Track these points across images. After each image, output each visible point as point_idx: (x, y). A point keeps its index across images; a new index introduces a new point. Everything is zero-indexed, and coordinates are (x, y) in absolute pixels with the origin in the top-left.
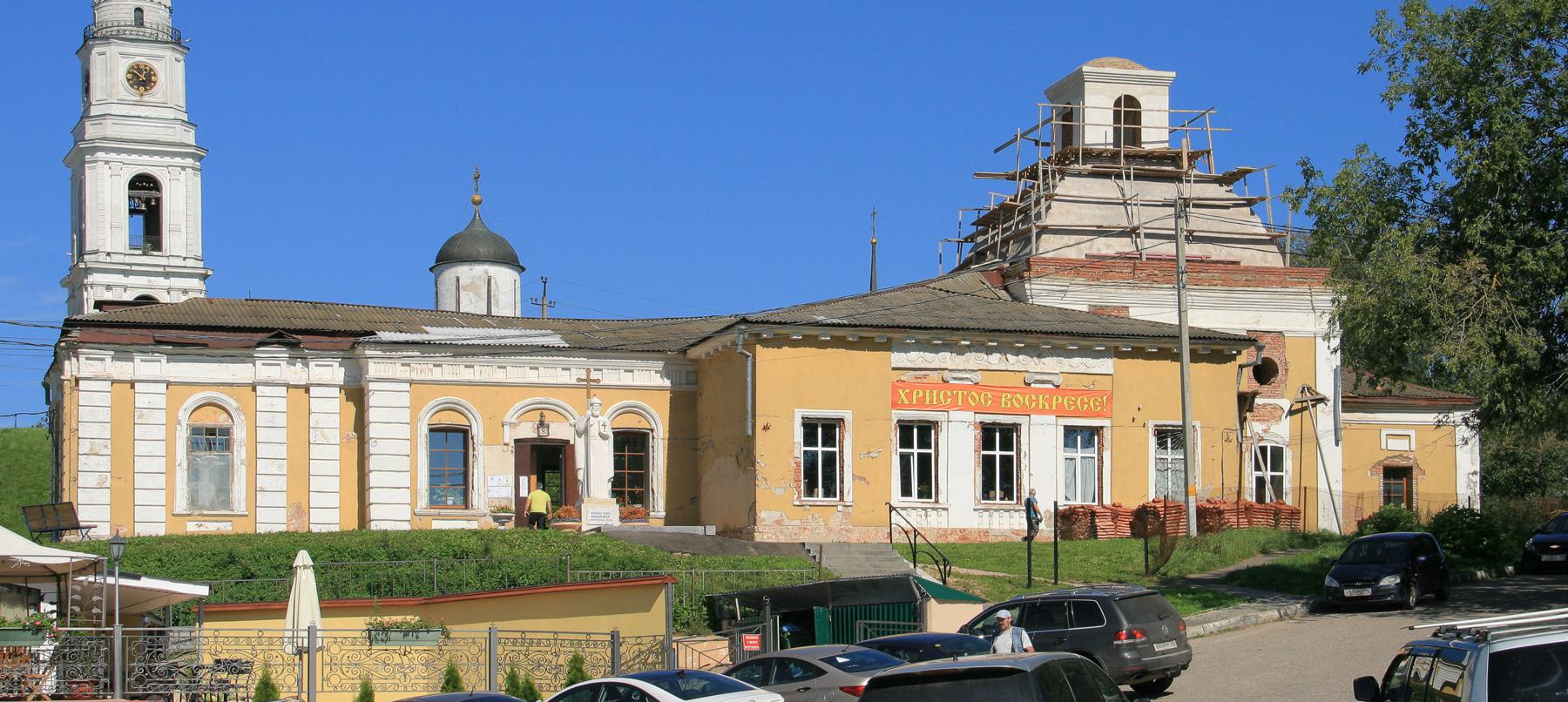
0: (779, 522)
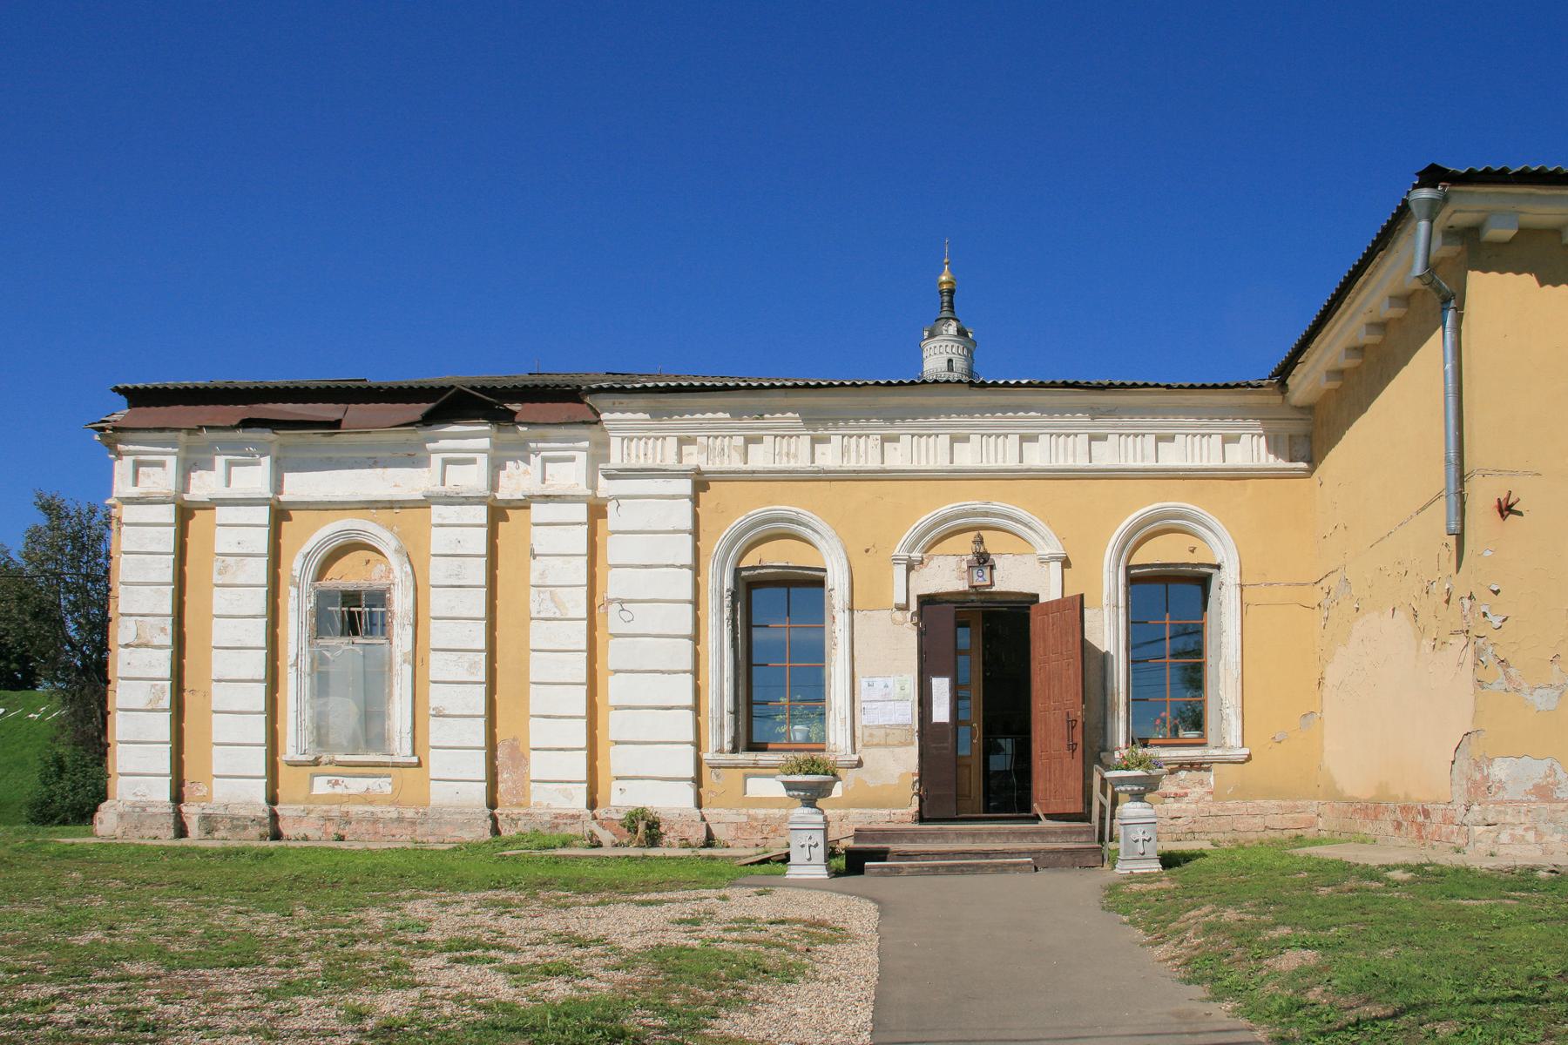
0: (1544, 792)
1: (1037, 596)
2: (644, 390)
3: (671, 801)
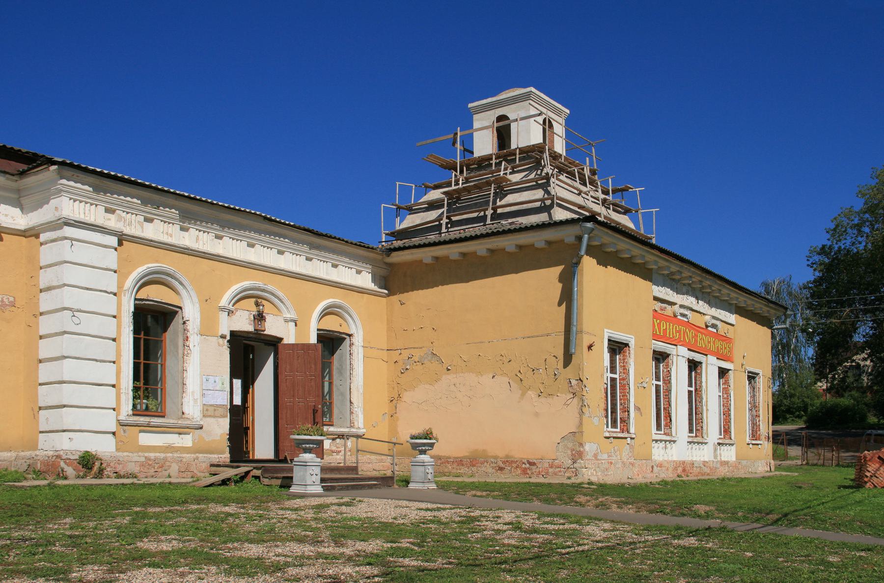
1: (281, 339)
2: (94, 172)
3: (103, 446)
